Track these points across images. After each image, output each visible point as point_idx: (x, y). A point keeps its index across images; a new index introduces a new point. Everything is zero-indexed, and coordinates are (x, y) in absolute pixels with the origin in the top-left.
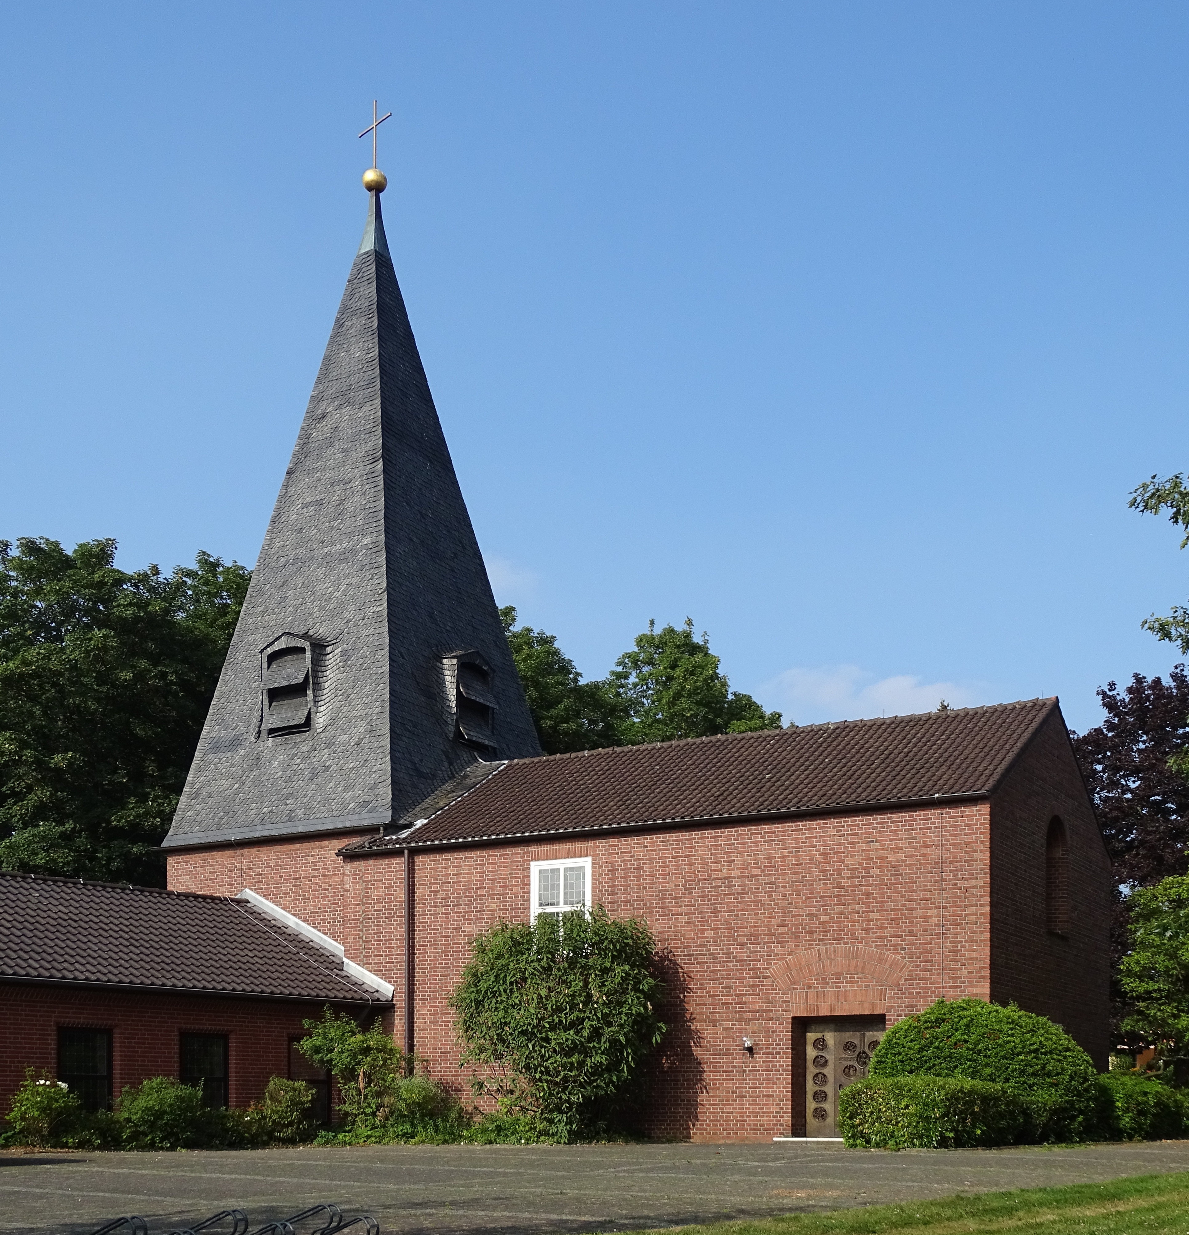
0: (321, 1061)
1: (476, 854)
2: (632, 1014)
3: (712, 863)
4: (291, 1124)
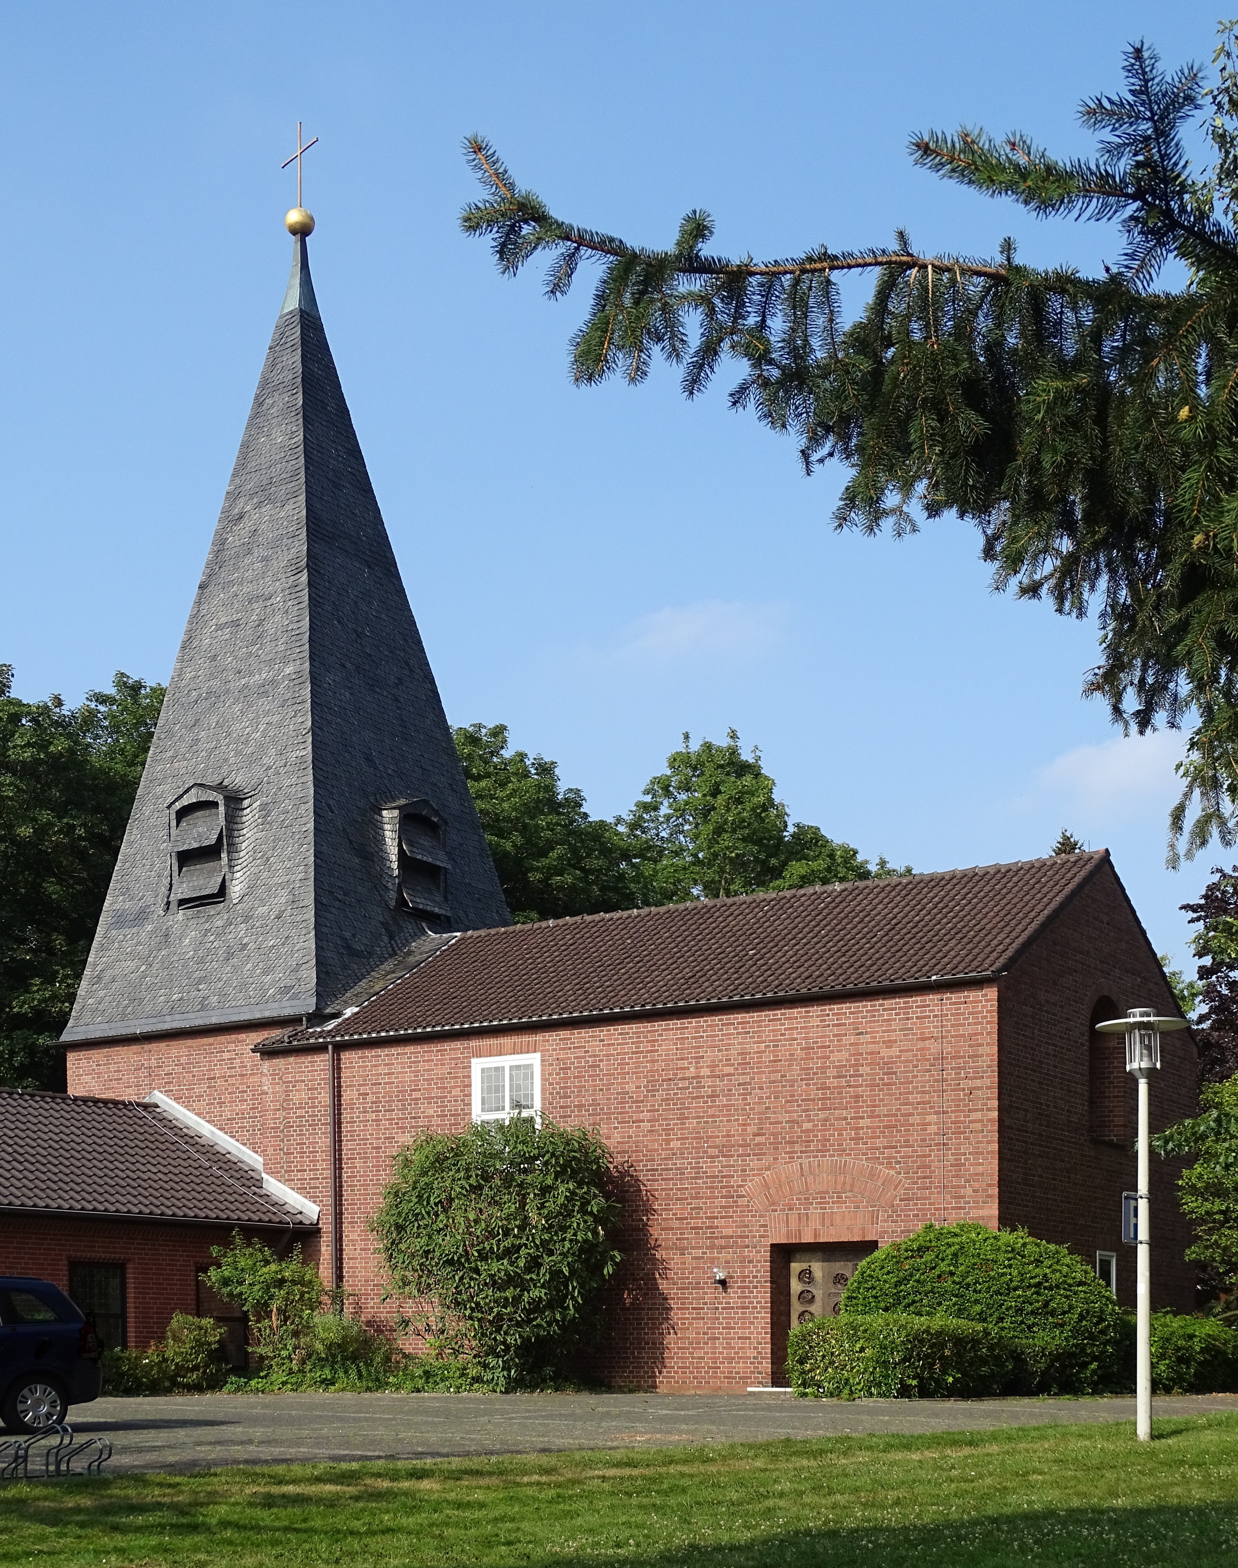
0: (230, 1294)
1: (409, 1049)
2: (577, 1241)
3: (678, 1059)
4: (196, 1368)
